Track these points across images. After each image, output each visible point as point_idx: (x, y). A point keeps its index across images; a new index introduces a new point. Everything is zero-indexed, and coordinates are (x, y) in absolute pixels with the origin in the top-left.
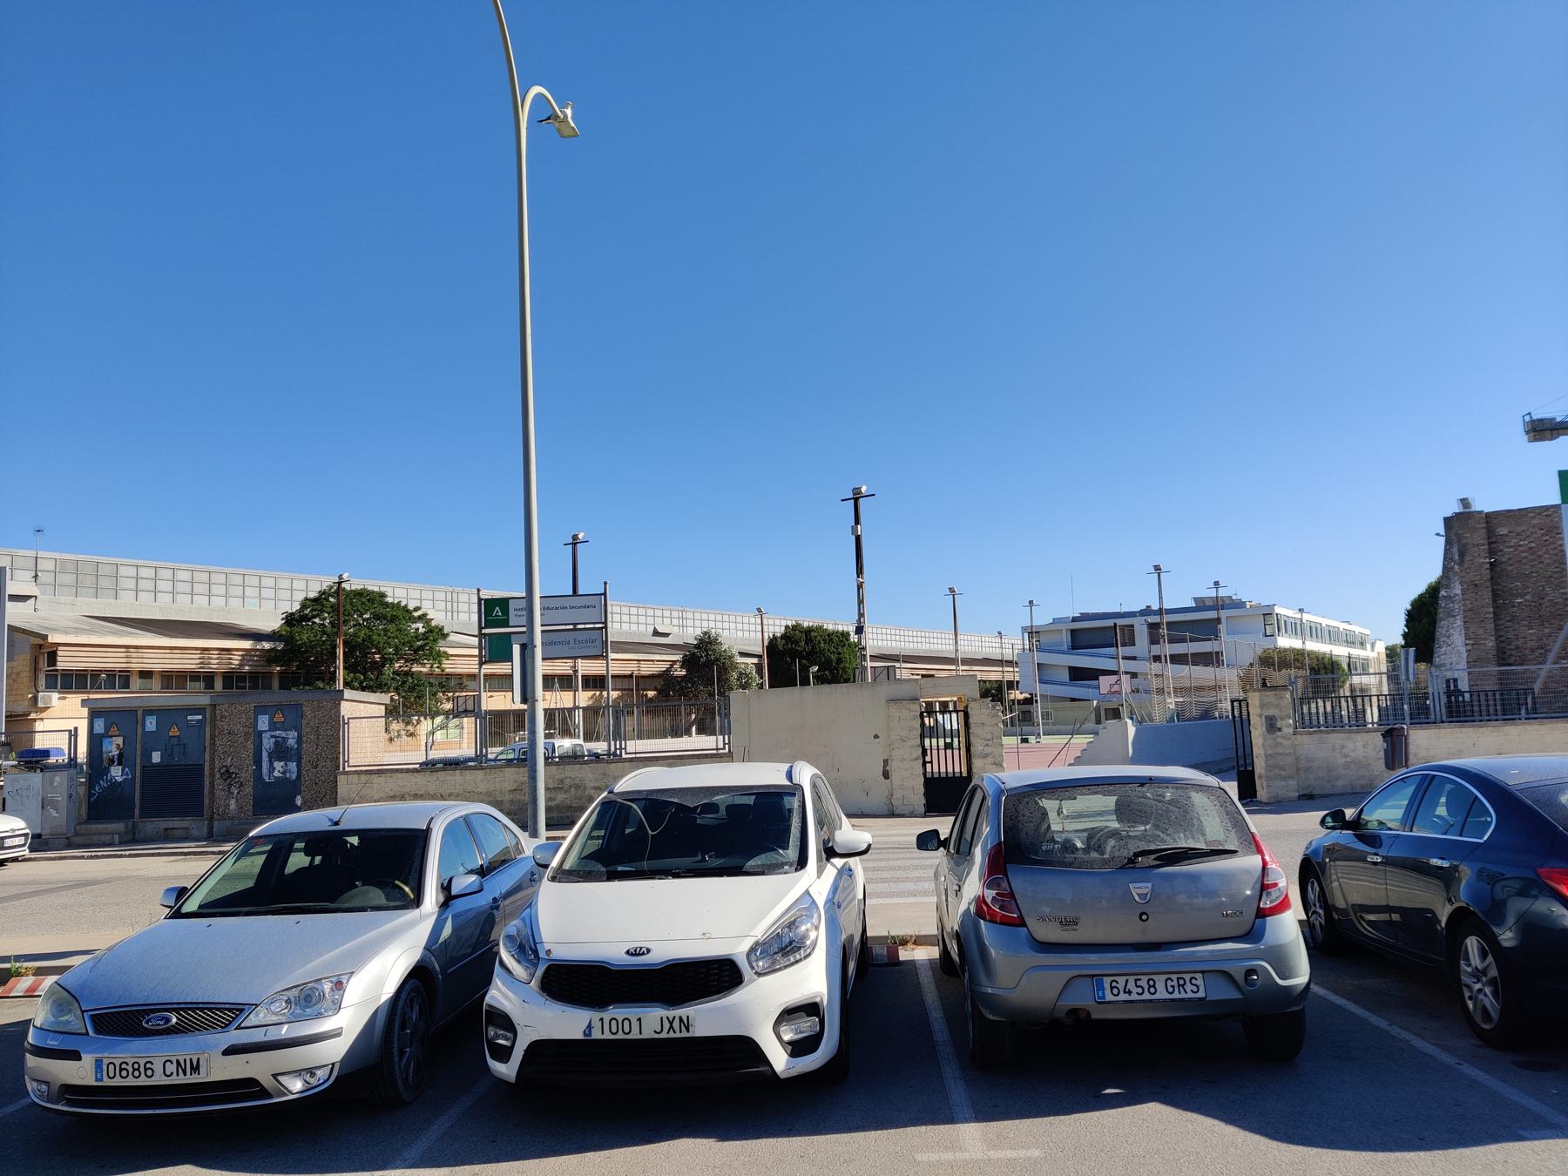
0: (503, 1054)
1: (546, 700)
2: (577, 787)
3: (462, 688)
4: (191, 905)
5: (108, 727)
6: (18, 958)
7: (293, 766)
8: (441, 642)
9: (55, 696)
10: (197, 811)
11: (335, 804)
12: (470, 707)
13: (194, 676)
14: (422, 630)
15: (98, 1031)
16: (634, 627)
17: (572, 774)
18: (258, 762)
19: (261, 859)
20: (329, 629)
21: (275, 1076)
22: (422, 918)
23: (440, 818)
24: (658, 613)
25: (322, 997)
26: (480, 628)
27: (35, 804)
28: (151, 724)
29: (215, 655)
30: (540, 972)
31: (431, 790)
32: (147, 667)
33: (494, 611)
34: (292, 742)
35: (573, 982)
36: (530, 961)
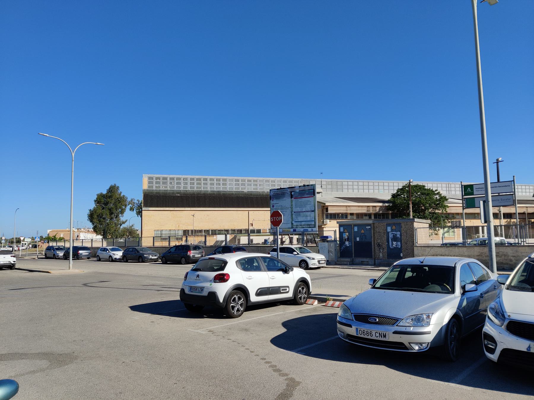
0: (492, 351)
1: (494, 222)
2: (505, 255)
3: (454, 218)
4: (378, 285)
5: (344, 230)
6: (328, 295)
7: (399, 243)
8: (445, 202)
9: (328, 221)
10: (370, 256)
11: (414, 257)
12: (458, 225)
13: (366, 215)
14: (438, 198)
15: (356, 320)
16: (524, 194)
17: (502, 250)
18: (388, 242)
19: (397, 273)
20: (406, 199)
21: (409, 343)
22: (455, 298)
23: (459, 263)
25: (423, 320)
26: (463, 196)
27: (327, 251)
28: (356, 229)
29: (371, 208)
30: (506, 323)
31: (447, 253)
32: (352, 212)
33: (467, 189)
34: (398, 236)
35: (518, 328)
36: (501, 319)
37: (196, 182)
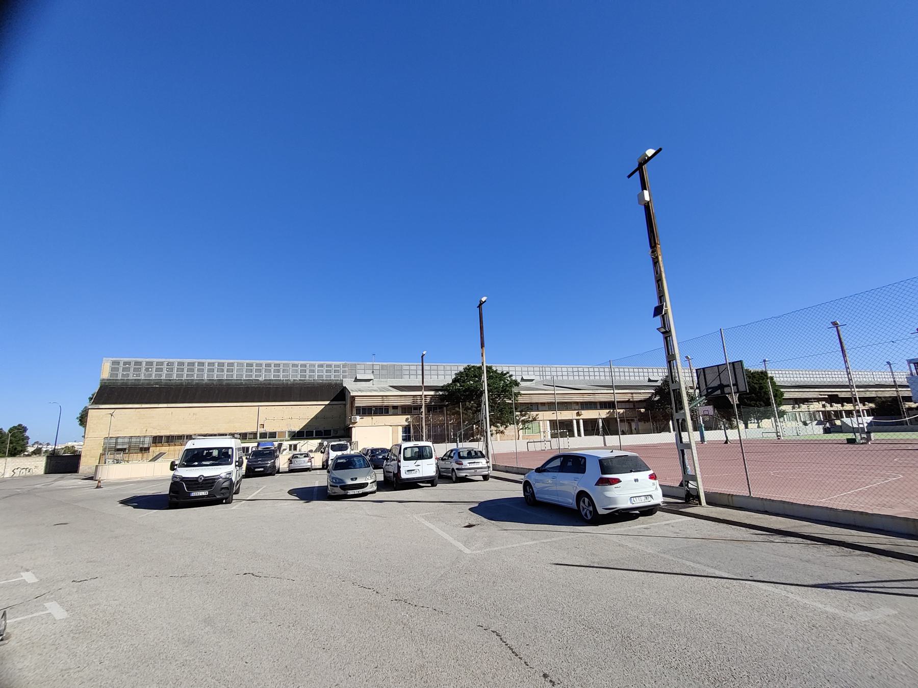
9: (358, 417)
16: (637, 378)
24: (650, 370)
32: (395, 404)
37: (186, 368)
